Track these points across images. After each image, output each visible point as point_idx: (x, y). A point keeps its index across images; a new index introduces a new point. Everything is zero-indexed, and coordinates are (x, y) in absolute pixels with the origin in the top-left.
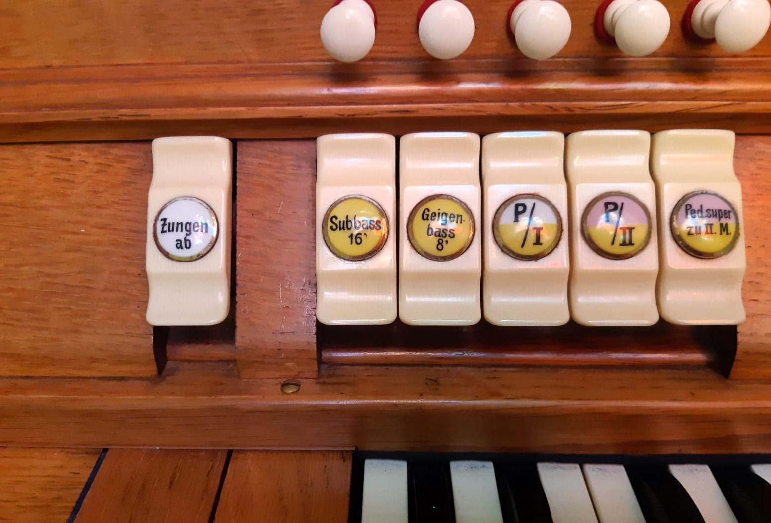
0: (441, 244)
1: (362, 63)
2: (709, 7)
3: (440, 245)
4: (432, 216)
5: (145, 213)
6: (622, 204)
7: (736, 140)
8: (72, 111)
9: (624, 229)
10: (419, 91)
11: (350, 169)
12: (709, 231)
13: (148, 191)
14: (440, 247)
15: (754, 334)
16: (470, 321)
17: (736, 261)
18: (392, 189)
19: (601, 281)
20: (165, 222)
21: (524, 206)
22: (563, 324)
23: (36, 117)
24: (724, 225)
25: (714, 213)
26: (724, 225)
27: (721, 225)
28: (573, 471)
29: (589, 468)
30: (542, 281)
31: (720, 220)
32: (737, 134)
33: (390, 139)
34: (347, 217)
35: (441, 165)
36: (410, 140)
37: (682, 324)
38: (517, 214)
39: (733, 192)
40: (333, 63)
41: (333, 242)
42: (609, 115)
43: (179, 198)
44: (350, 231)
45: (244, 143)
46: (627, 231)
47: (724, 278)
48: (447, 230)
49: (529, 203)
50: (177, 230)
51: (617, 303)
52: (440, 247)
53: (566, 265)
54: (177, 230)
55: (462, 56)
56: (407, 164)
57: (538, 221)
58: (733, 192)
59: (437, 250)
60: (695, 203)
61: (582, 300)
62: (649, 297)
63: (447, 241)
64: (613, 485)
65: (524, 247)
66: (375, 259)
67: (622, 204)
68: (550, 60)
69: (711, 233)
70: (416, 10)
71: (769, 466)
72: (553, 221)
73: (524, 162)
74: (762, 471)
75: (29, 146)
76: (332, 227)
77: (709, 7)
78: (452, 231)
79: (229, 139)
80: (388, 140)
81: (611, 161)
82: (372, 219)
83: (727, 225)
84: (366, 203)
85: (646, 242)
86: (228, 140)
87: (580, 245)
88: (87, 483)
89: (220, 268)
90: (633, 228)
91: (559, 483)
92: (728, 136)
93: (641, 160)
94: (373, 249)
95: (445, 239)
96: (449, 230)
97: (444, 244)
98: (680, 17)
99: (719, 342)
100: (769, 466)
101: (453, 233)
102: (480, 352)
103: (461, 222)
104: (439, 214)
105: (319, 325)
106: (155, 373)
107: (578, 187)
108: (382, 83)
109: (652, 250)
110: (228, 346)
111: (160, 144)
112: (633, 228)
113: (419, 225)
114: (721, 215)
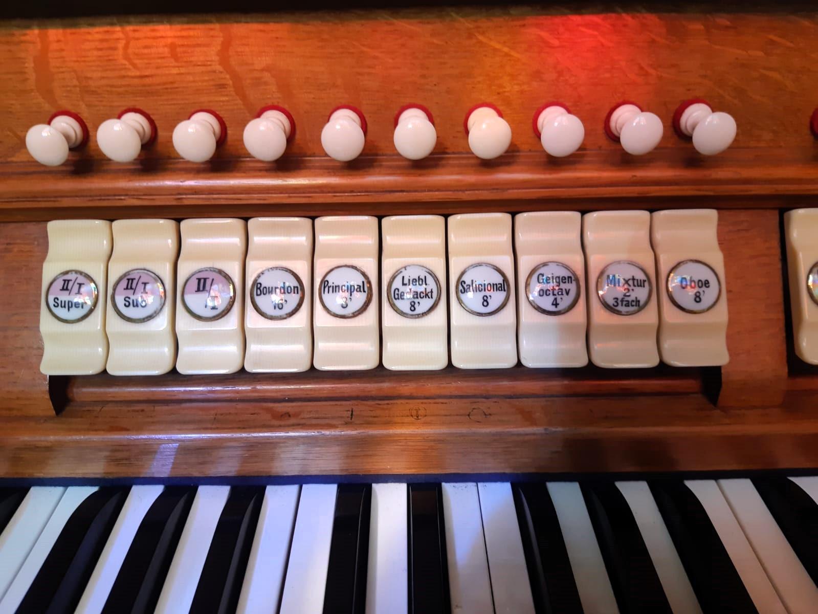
4: (547, 280)
6: (425, 277)
7: (719, 213)
19: (264, 337)
28: (711, 483)
33: (507, 217)
37: (676, 366)
43: (468, 267)
44: (486, 295)
50: (65, 302)
52: (413, 308)
59: (482, 306)
61: (668, 344)
62: (651, 344)
67: (425, 277)
71: (817, 478)
72: (187, 297)
76: (461, 290)
82: (684, 276)
87: (386, 308)
88: (311, 476)
89: (99, 328)
91: (705, 492)
92: (711, 215)
94: (264, 313)
97: (416, 306)
98: (669, 123)
99: (709, 378)
100: (817, 478)
102: (226, 385)
103: (571, 282)
104: (553, 277)
111: (54, 226)
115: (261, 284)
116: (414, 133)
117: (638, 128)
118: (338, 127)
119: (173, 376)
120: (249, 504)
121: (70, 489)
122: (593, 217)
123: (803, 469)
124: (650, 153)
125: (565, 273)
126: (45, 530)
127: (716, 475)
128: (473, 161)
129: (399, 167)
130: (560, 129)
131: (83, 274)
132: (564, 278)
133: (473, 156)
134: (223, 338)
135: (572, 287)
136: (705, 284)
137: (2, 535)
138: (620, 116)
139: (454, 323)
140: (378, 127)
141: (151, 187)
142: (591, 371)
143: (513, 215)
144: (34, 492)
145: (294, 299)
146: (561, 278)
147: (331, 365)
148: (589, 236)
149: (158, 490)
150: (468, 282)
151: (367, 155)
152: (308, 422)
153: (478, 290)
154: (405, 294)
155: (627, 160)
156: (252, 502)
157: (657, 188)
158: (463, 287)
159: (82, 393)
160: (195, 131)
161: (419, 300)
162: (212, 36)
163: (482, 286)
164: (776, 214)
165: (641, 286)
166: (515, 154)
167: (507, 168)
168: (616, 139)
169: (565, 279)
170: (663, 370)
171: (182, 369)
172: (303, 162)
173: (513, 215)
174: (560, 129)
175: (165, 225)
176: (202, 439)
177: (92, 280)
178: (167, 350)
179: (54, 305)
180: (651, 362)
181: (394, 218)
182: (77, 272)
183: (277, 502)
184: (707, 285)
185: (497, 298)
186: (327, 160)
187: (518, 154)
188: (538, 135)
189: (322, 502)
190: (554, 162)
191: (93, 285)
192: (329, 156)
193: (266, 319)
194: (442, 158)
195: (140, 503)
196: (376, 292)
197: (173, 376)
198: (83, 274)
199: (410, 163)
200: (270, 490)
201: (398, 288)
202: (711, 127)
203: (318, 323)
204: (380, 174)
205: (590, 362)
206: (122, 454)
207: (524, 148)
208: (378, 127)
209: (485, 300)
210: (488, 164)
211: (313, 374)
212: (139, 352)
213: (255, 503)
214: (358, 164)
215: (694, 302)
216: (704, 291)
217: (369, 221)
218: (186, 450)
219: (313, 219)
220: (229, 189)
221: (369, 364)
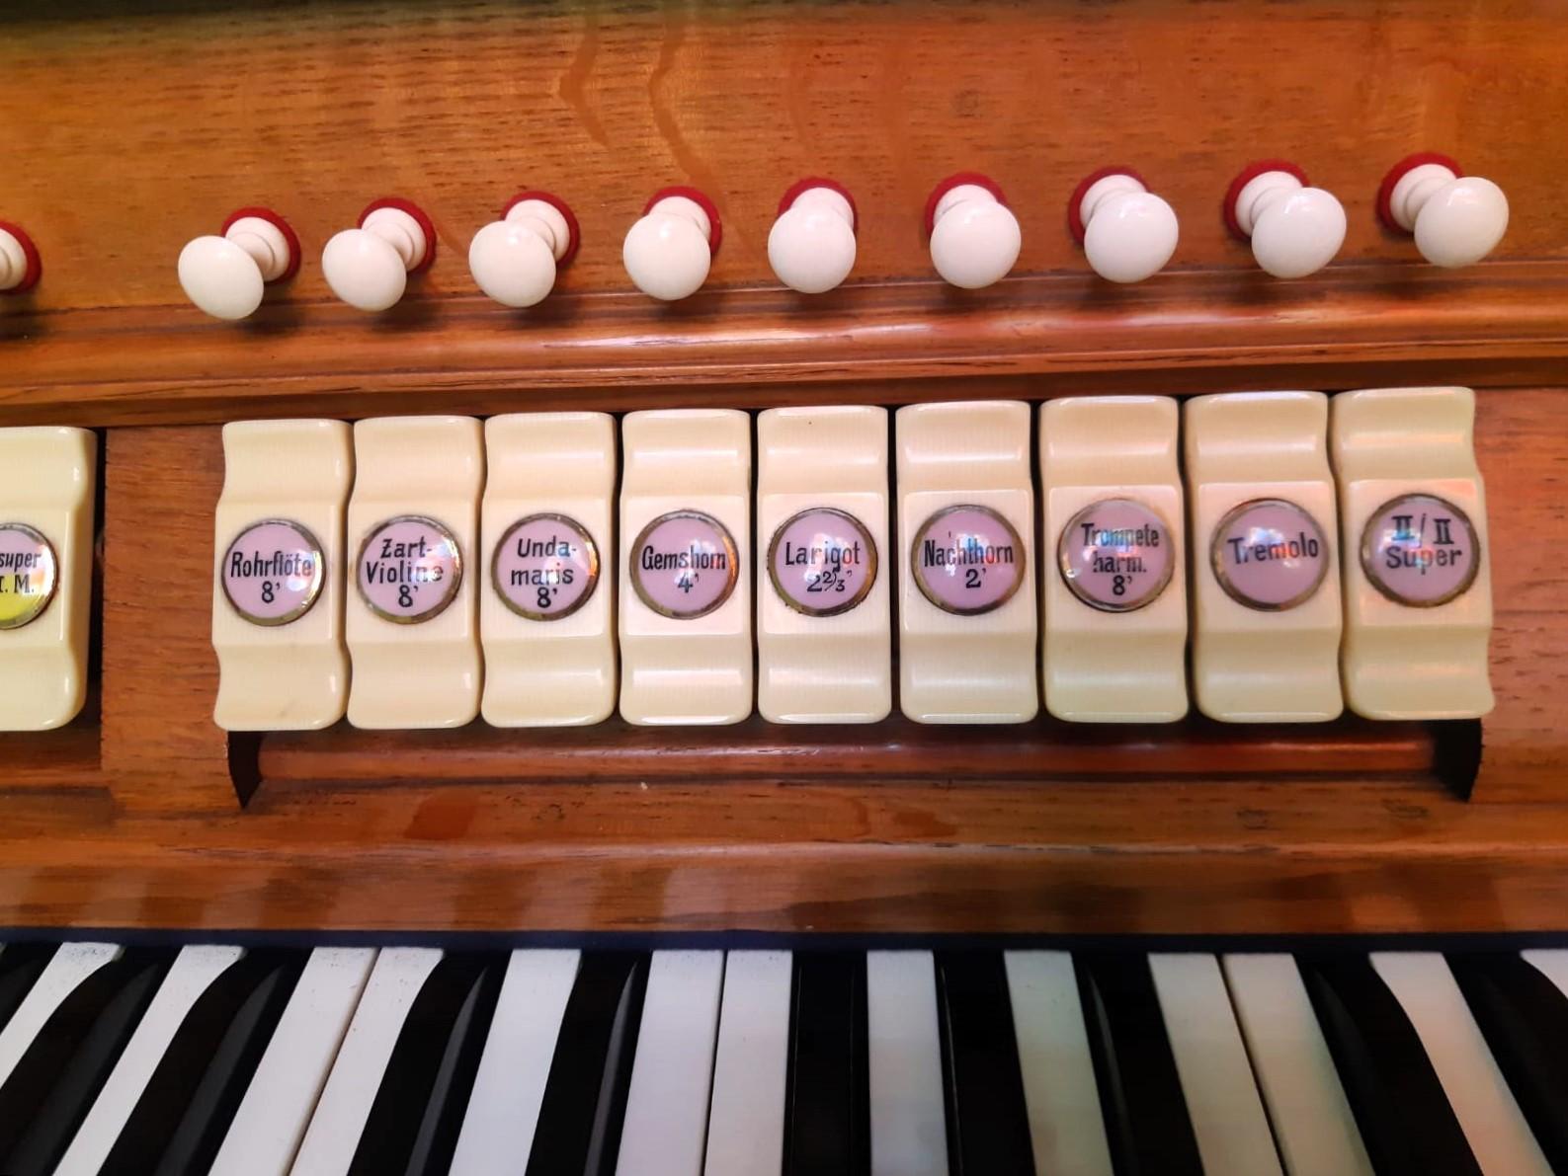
1: (844, 286)
3: (1119, 586)
5: (211, 542)
7: (1478, 397)
10: (598, 339)
11: (274, 473)
13: (215, 506)
14: (267, 597)
16: (1018, 715)
17: (1476, 608)
18: (1027, 495)
20: (385, 551)
22: (1170, 721)
25: (9, 560)
26: (22, 578)
27: (17, 577)
28: (1204, 964)
29: (1236, 962)
30: (1301, 644)
31: (15, 570)
33: (739, 419)
34: (257, 553)
35: (417, 464)
36: (1203, 406)
39: (1471, 496)
40: (1088, 277)
41: (646, 587)
42: (173, 400)
45: (119, 433)
47: (1451, 640)
51: (1266, 682)
52: (267, 597)
53: (1334, 621)
54: (255, 574)
55: (1487, 259)
56: (1052, 452)
58: (1471, 496)
59: (266, 604)
64: (1274, 987)
66: (1001, 613)
68: (1005, 280)
70: (225, 218)
73: (1111, 453)
74: (1551, 964)
75: (163, 429)
78: (568, 573)
79: (609, 413)
80: (1167, 405)
81: (1261, 448)
84: (1255, 511)
85: (451, 597)
86: (607, 415)
89: (61, 638)
91: (1183, 984)
92: (1462, 397)
93: (1311, 445)
99: (1452, 752)
100: (1564, 954)
101: (569, 577)
107: (1201, 487)
108: (880, 318)
109: (1175, 598)
111: (235, 432)
113: (510, 561)
114: (19, 563)
115: (241, 554)
116: (976, 232)
117: (1130, 225)
118: (513, 241)
120: (471, 987)
121: (388, 954)
123: (907, 935)
124: (1314, 277)
127: (1220, 946)
128: (783, 301)
129: (643, 314)
130: (1130, 225)
131: (559, 518)
134: (575, 650)
135: (1152, 558)
137: (4, 1033)
138: (1414, 188)
139: (907, 628)
140: (897, 220)
141: (428, 356)
143: (1182, 399)
144: (66, 949)
145: (715, 580)
147: (665, 715)
150: (249, 556)
151: (715, 282)
153: (242, 573)
154: (544, 574)
155: (1105, 294)
156: (629, 979)
158: (933, 555)
159: (270, 763)
161: (1131, 574)
162: (100, 61)
163: (244, 571)
164: (883, 413)
165: (520, 573)
170: (1351, 724)
171: (632, 714)
172: (579, 303)
173: (1182, 399)
174: (976, 232)
175: (328, 428)
177: (451, 535)
178: (600, 678)
179: (1389, 564)
180: (1328, 710)
181: (1359, 395)
182: (408, 519)
183: (676, 986)
185: (999, 574)
186: (484, 304)
190: (958, 301)
191: (449, 544)
192: (641, 291)
193: (1156, 604)
194: (723, 294)
195: (193, 973)
198: (559, 518)
200: (661, 960)
202: (1459, 211)
206: (498, 883)
208: (897, 220)
209: (1118, 585)
211: (896, 725)
212: (411, 685)
213: (483, 988)
214: (554, 310)
215: (1112, 593)
216: (984, 570)
217: (598, 422)
219: (1331, 394)
220: (571, 354)
221: (594, 712)
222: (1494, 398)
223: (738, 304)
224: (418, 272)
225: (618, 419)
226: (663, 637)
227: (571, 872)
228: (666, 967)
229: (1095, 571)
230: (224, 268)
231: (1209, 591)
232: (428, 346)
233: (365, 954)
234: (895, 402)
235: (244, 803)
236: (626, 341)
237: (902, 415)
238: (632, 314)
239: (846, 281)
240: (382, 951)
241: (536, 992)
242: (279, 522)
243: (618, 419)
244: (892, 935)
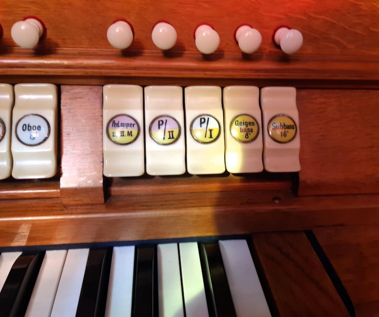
0: (247, 135)
2: (279, 37)
6: (166, 120)
7: (297, 92)
8: (186, 72)
9: (169, 132)
12: (122, 135)
14: (247, 137)
15: (310, 177)
21: (162, 121)
23: (314, 76)
24: (130, 132)
26: (130, 132)
32: (297, 88)
38: (201, 123)
46: (122, 133)
48: (249, 129)
49: (206, 118)
52: (247, 137)
57: (169, 128)
60: (116, 120)
63: (250, 134)
65: (206, 137)
67: (166, 120)
69: (123, 135)
77: (279, 37)
80: (179, 89)
83: (131, 132)
90: (212, 130)
92: (292, 91)
95: (249, 133)
96: (250, 129)
97: (249, 135)
103: (254, 125)
105: (104, 178)
106: (104, 202)
110: (56, 189)
112: (212, 130)
118: (117, 31)
119: (187, 175)
122: (266, 90)
125: (251, 120)
126: (61, 279)
131: (281, 115)
132: (250, 123)
133: (198, 52)
136: (38, 128)
142: (264, 176)
146: (248, 123)
148: (264, 100)
149: (18, 254)
150: (117, 122)
152: (188, 205)
157: (211, 73)
159: (115, 189)
160: (25, 27)
166: (57, 48)
167: (179, 59)
168: (278, 46)
169: (242, 123)
176: (57, 219)
184: (39, 129)
187: (58, 48)
188: (237, 43)
189: (80, 259)
190: (247, 57)
196: (85, 129)
197: (187, 175)
199: (201, 56)
200: (49, 253)
201: (39, 125)
203: (267, 145)
204: (56, 58)
205: (264, 170)
207: (271, 49)
210: (207, 58)
211: (145, 176)
218: (35, 227)
222: (303, 93)
223: (147, 54)
224: (43, 37)
225: (222, 88)
226: (28, 152)
227: (136, 222)
228: (50, 255)
229: (121, 136)
230: (119, 34)
231: (268, 140)
232: (137, 62)
233: (63, 252)
234: (185, 85)
235: (105, 201)
236: (151, 63)
237: (186, 89)
238: (108, 55)
239: (216, 51)
240: (69, 250)
241: (124, 261)
242: (283, 115)
243: (222, 88)
244: (162, 239)
